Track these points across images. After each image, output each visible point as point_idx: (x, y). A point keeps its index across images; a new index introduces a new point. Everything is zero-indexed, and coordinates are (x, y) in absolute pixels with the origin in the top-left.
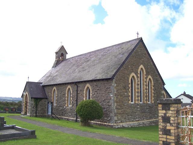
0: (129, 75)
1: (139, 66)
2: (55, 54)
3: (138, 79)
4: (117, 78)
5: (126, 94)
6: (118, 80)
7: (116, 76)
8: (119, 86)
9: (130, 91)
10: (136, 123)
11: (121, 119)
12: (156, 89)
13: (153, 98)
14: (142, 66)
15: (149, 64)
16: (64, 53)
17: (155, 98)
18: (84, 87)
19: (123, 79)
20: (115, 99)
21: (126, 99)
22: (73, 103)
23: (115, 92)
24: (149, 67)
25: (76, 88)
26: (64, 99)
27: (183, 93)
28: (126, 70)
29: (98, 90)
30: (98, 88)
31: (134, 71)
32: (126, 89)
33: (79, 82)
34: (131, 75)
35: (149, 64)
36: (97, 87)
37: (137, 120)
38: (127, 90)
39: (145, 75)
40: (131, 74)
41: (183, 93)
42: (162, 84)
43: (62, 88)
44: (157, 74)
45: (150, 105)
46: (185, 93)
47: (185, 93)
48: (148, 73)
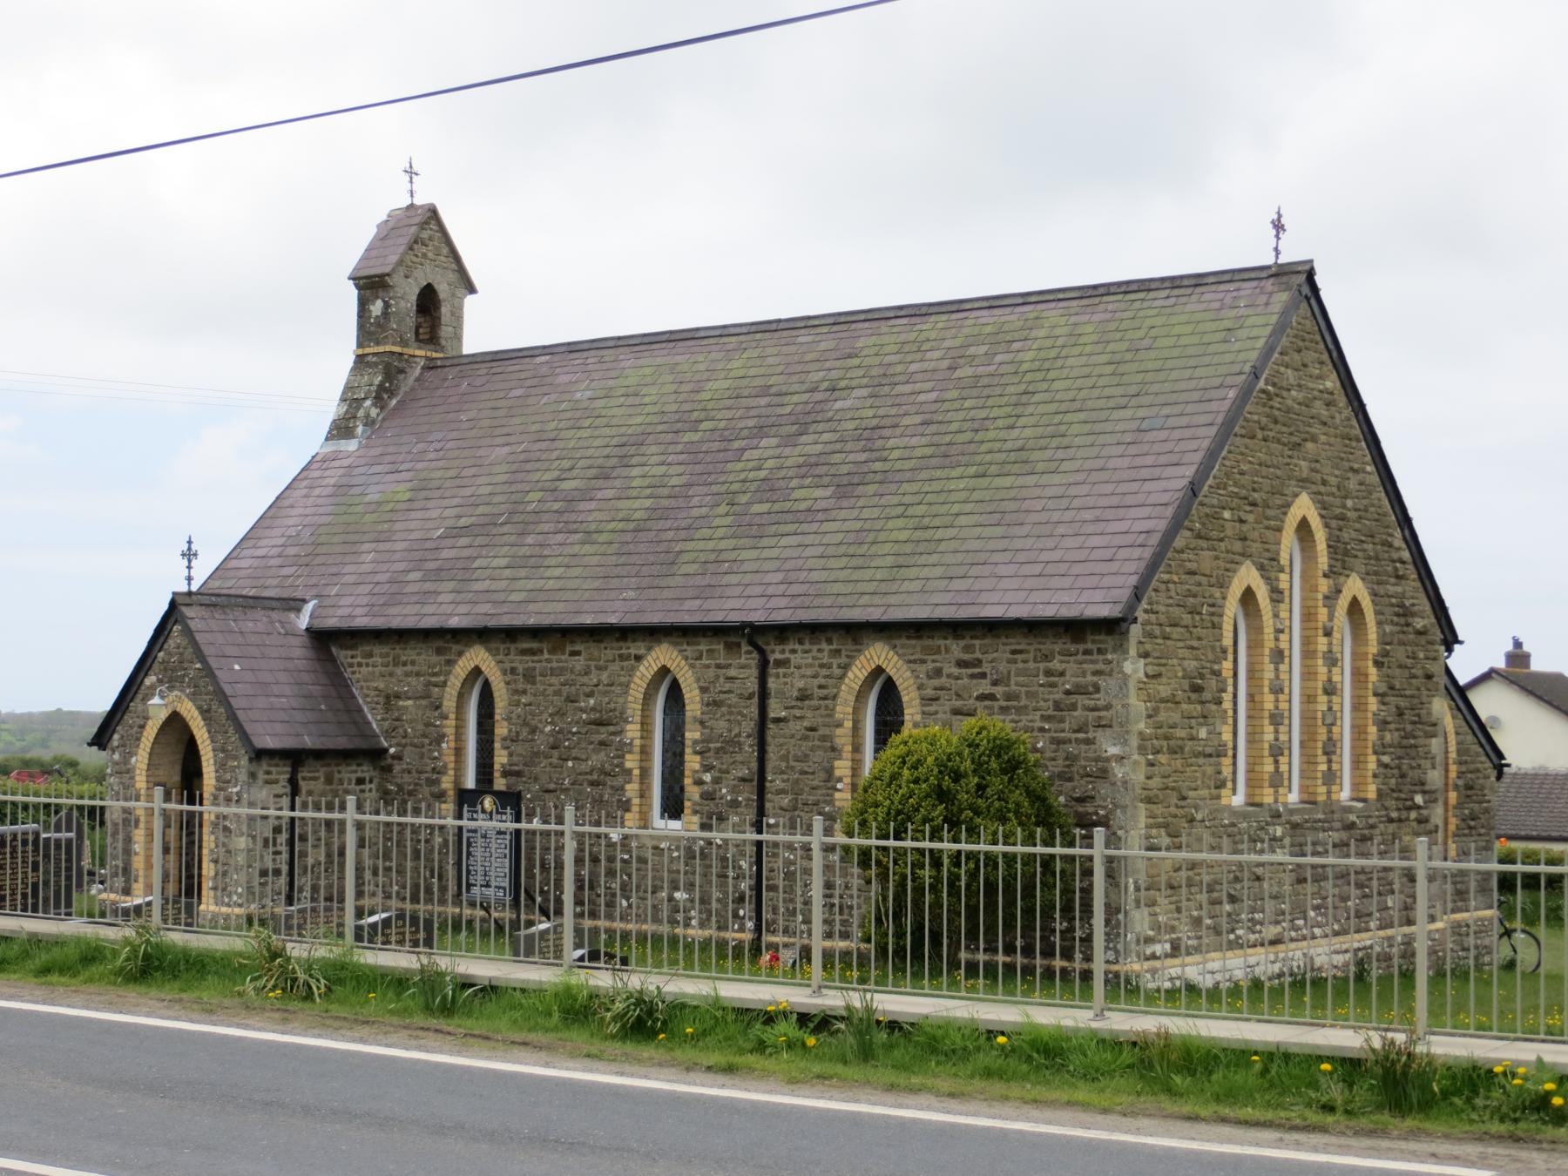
0: (1223, 585)
1: (1288, 505)
2: (352, 293)
3: (1276, 616)
4: (1153, 617)
5: (1203, 733)
6: (1157, 631)
7: (1144, 605)
8: (1160, 675)
9: (1225, 711)
10: (1263, 962)
11: (1173, 929)
12: (1392, 688)
13: (1372, 764)
14: (1304, 506)
15: (1352, 484)
16: (443, 290)
17: (1386, 759)
18: (837, 672)
19: (1187, 618)
20: (1142, 778)
21: (1204, 774)
22: (708, 796)
23: (1142, 726)
24: (1349, 503)
25: (754, 672)
26: (597, 759)
27: (1501, 664)
28: (1204, 544)
29: (982, 697)
30: (984, 687)
31: (1255, 547)
32: (1207, 695)
33: (783, 632)
34: (1236, 581)
35: (1352, 484)
36: (973, 676)
37: (1271, 931)
38: (1214, 707)
39: (1325, 576)
40: (1235, 571)
41: (1501, 664)
42: (1439, 636)
43: (579, 663)
44: (1406, 555)
45: (1353, 818)
46: (1518, 657)
47: (1518, 657)
48: (1346, 553)
